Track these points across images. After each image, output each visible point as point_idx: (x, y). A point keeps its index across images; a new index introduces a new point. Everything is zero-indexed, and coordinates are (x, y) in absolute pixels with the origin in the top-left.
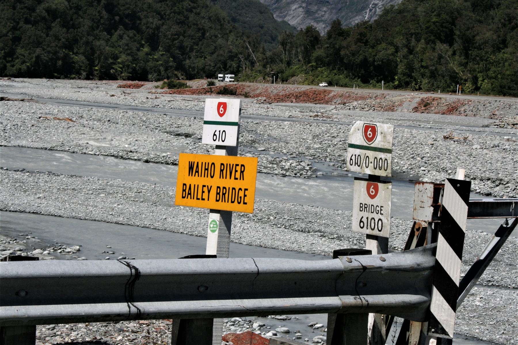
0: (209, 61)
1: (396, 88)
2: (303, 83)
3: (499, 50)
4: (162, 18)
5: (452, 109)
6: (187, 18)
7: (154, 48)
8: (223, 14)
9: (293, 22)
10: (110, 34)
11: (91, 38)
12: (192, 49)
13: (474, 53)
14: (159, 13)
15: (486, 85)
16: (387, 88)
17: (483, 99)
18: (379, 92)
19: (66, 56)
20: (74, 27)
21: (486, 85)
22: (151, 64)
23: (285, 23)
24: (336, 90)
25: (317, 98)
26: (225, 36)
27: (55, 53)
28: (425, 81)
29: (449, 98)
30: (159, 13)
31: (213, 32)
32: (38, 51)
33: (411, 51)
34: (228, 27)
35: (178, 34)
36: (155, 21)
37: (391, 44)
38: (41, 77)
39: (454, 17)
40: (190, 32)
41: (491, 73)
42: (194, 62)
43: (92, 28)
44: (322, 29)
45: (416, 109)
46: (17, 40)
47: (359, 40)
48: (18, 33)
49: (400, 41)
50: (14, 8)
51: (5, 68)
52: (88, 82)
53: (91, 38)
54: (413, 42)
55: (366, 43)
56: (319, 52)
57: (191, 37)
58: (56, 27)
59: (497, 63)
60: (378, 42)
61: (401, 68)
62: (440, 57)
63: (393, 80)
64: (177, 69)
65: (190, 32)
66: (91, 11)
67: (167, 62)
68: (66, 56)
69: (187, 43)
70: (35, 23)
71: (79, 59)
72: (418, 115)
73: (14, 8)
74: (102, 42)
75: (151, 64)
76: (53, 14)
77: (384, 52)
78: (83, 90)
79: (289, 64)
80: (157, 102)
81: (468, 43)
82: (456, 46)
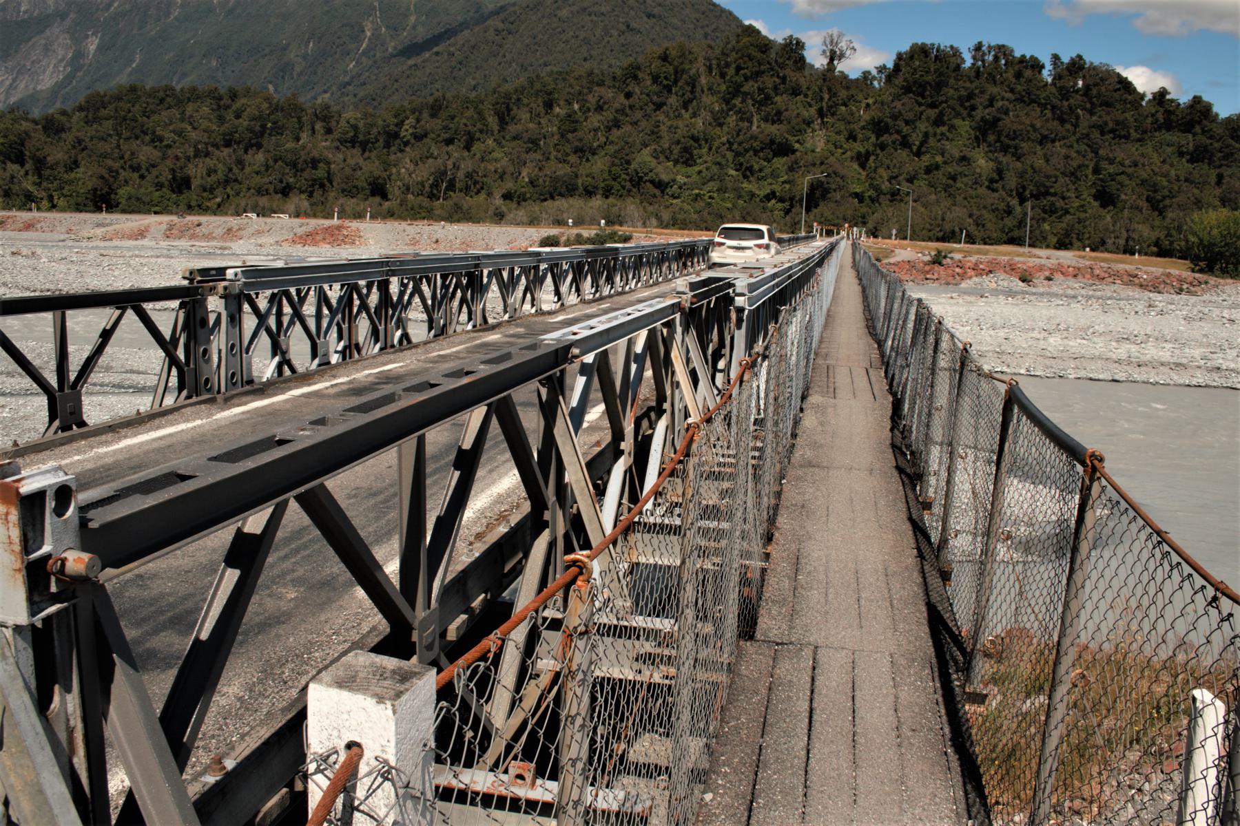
3: (72, 169)
5: (29, 226)
13: (46, 173)
21: (62, 203)
29: (24, 216)
39: (23, 139)
41: (65, 192)
59: (71, 182)
62: (12, 177)
82: (27, 166)
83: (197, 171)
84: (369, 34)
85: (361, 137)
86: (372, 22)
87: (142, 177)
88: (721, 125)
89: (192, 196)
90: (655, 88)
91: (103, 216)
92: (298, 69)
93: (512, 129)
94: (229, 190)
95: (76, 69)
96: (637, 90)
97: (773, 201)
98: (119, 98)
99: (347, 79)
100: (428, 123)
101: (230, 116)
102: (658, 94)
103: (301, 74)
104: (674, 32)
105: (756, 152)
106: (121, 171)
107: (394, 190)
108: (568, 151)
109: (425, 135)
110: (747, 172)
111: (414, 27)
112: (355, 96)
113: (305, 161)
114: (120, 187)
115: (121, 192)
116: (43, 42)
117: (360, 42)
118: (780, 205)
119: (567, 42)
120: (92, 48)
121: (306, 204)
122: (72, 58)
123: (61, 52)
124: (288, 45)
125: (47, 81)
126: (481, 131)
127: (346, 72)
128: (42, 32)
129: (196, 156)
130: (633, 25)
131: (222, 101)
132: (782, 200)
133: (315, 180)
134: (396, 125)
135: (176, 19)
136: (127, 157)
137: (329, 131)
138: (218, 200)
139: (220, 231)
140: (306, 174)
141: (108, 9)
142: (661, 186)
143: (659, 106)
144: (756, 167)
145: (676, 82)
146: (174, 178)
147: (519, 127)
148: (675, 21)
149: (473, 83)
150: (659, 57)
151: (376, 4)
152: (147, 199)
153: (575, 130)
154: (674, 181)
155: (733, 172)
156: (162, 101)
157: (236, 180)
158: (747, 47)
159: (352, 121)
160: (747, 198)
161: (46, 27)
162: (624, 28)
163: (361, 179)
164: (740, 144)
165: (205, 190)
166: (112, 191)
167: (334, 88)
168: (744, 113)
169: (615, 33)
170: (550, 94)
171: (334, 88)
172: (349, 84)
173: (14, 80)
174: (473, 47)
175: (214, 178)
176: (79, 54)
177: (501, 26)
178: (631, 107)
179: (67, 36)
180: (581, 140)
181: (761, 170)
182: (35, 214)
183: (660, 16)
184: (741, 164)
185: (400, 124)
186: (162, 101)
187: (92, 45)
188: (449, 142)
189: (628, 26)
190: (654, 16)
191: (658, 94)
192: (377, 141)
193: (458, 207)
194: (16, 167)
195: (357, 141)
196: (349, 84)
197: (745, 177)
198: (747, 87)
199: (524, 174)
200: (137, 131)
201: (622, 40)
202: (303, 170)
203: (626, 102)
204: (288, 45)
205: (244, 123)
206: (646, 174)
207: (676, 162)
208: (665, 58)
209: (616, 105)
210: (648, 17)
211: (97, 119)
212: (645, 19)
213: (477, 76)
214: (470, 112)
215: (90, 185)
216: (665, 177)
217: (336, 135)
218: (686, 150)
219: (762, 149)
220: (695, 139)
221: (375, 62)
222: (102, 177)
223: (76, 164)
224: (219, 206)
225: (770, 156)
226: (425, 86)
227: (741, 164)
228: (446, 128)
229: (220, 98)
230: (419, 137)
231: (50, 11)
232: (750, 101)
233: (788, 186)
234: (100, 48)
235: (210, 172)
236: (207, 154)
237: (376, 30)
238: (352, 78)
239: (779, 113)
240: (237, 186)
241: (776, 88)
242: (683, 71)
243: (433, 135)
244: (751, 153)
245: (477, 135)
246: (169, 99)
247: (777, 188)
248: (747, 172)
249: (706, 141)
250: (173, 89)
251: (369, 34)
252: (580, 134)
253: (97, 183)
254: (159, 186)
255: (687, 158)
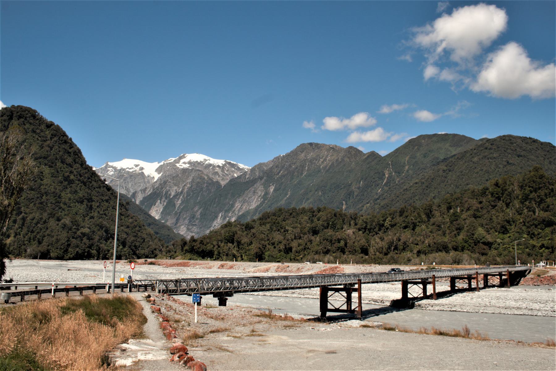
0: (146, 251)
1: (214, 260)
2: (180, 259)
3: (250, 245)
4: (127, 235)
5: (231, 267)
6: (137, 234)
7: (124, 246)
8: (152, 232)
9: (182, 233)
10: (107, 241)
11: (99, 244)
12: (139, 247)
13: (240, 247)
14: (126, 233)
15: (245, 258)
16: (211, 260)
17: (244, 263)
18: (207, 262)
19: (89, 251)
20: (92, 239)
21: (245, 258)
22: (123, 253)
23: (179, 234)
24: (192, 262)
25: (184, 265)
26: (153, 241)
27: (84, 250)
28: (225, 257)
29: (230, 263)
30: (126, 233)
31: (148, 239)
32: (77, 249)
33: (219, 247)
34: (154, 237)
35: (134, 241)
36: (125, 236)
37: (212, 244)
38: (78, 260)
39: (235, 233)
40: (139, 240)
41: (247, 254)
42: (140, 251)
43: (99, 240)
44: (188, 238)
45: (219, 268)
46: (69, 245)
47: (201, 243)
48: (69, 242)
49: (215, 243)
50: (68, 233)
51: (64, 256)
52: (98, 261)
53: (99, 244)
54: (220, 243)
55: (203, 244)
56: (186, 247)
57: (139, 241)
58: (85, 240)
59: (249, 250)
60: (208, 243)
61: (216, 253)
62: (229, 248)
63: (213, 257)
64: (133, 254)
65: (139, 240)
66: (99, 233)
67: (130, 252)
68: (89, 251)
69: (138, 244)
70: (76, 238)
71: (94, 252)
72: (219, 270)
73: (68, 233)
74: (103, 245)
75: (123, 253)
76: (84, 234)
77: (209, 247)
78: (96, 265)
79: (175, 252)
80: (125, 269)
81: (239, 243)
82: (235, 244)
83: (294, 244)
84: (387, 176)
85: (368, 227)
86: (388, 170)
87: (275, 247)
88: (520, 214)
89: (292, 255)
90: (493, 199)
91: (257, 264)
92: (356, 194)
93: (432, 220)
94: (305, 252)
95: (265, 200)
96: (484, 200)
97: (544, 249)
98: (274, 214)
99: (377, 197)
100: (399, 219)
101: (315, 220)
102: (494, 201)
103: (357, 196)
104: (533, 162)
105: (536, 226)
106: (267, 245)
107: (371, 250)
108: (454, 229)
109: (395, 225)
110: (532, 236)
111: (408, 171)
112: (379, 205)
113: (335, 240)
114: (266, 251)
115: (266, 253)
116: (253, 189)
117: (383, 180)
118: (547, 250)
119: (477, 173)
120: (272, 190)
121: (332, 258)
122: (264, 195)
123: (260, 193)
124: (352, 183)
125: (253, 205)
126: (419, 222)
127: (377, 194)
128: (253, 185)
129: (295, 238)
130: (510, 161)
131: (313, 213)
132: (547, 248)
133: (339, 248)
134: (383, 221)
135: (305, 176)
136: (270, 239)
137: (356, 224)
138: (301, 256)
139: (295, 269)
140: (335, 245)
141: (278, 174)
142: (489, 245)
143: (494, 207)
144: (536, 233)
145: (503, 194)
146: (286, 248)
147: (435, 219)
148: (533, 157)
149: (433, 195)
150: (495, 185)
151: (390, 162)
152: (275, 256)
153: (457, 220)
154: (496, 241)
155: (525, 236)
156: (291, 214)
157: (308, 248)
158: (532, 177)
159: (365, 220)
160: (530, 248)
161: (254, 184)
162: (506, 163)
163: (357, 246)
164: (528, 222)
165: (297, 252)
166: (263, 253)
167: (371, 201)
168: (530, 208)
169: (501, 166)
170: (449, 203)
171: (371, 201)
172: (378, 199)
173: (242, 206)
174: (433, 179)
175: (301, 247)
176: (266, 194)
177: (445, 168)
178: (481, 208)
179: (262, 186)
180: (458, 224)
181: (538, 234)
182: (235, 263)
183: (524, 156)
184: (529, 232)
185: (384, 221)
186: (291, 214)
187: (272, 189)
188: (405, 227)
189: (508, 162)
190: (521, 156)
191: (494, 201)
192: (375, 228)
193: (392, 258)
194: (231, 245)
195: (366, 229)
196: (378, 199)
197: (532, 238)
198: (531, 196)
199: (426, 242)
200: (279, 228)
201: (505, 169)
202: (334, 243)
203: (479, 206)
204: (352, 183)
205: (321, 222)
206: (481, 239)
207: (499, 232)
208: (497, 185)
209: (474, 208)
210: (518, 157)
211: (264, 224)
212: (517, 158)
213: (435, 192)
214: (415, 214)
215: (255, 251)
216: (490, 240)
217: (358, 226)
218: (503, 227)
219: (539, 224)
220: (508, 222)
221: (390, 188)
222: (260, 248)
223: (251, 243)
224: (302, 258)
225: (543, 227)
226: (411, 198)
227: (529, 232)
228: (404, 221)
229: (314, 212)
230: (392, 226)
231: (257, 177)
232: (533, 202)
233: (550, 241)
234: (274, 190)
235: (299, 245)
236: (300, 238)
237: (390, 174)
238: (379, 196)
239: (548, 207)
240: (309, 251)
241: (546, 195)
242: (506, 190)
243: (399, 225)
244: (534, 226)
245: (418, 224)
246: (294, 213)
247: (545, 243)
248: (532, 236)
249: (514, 222)
250: (295, 209)
251: (387, 176)
252: (458, 222)
253: (258, 250)
254: (280, 251)
255: (504, 231)
